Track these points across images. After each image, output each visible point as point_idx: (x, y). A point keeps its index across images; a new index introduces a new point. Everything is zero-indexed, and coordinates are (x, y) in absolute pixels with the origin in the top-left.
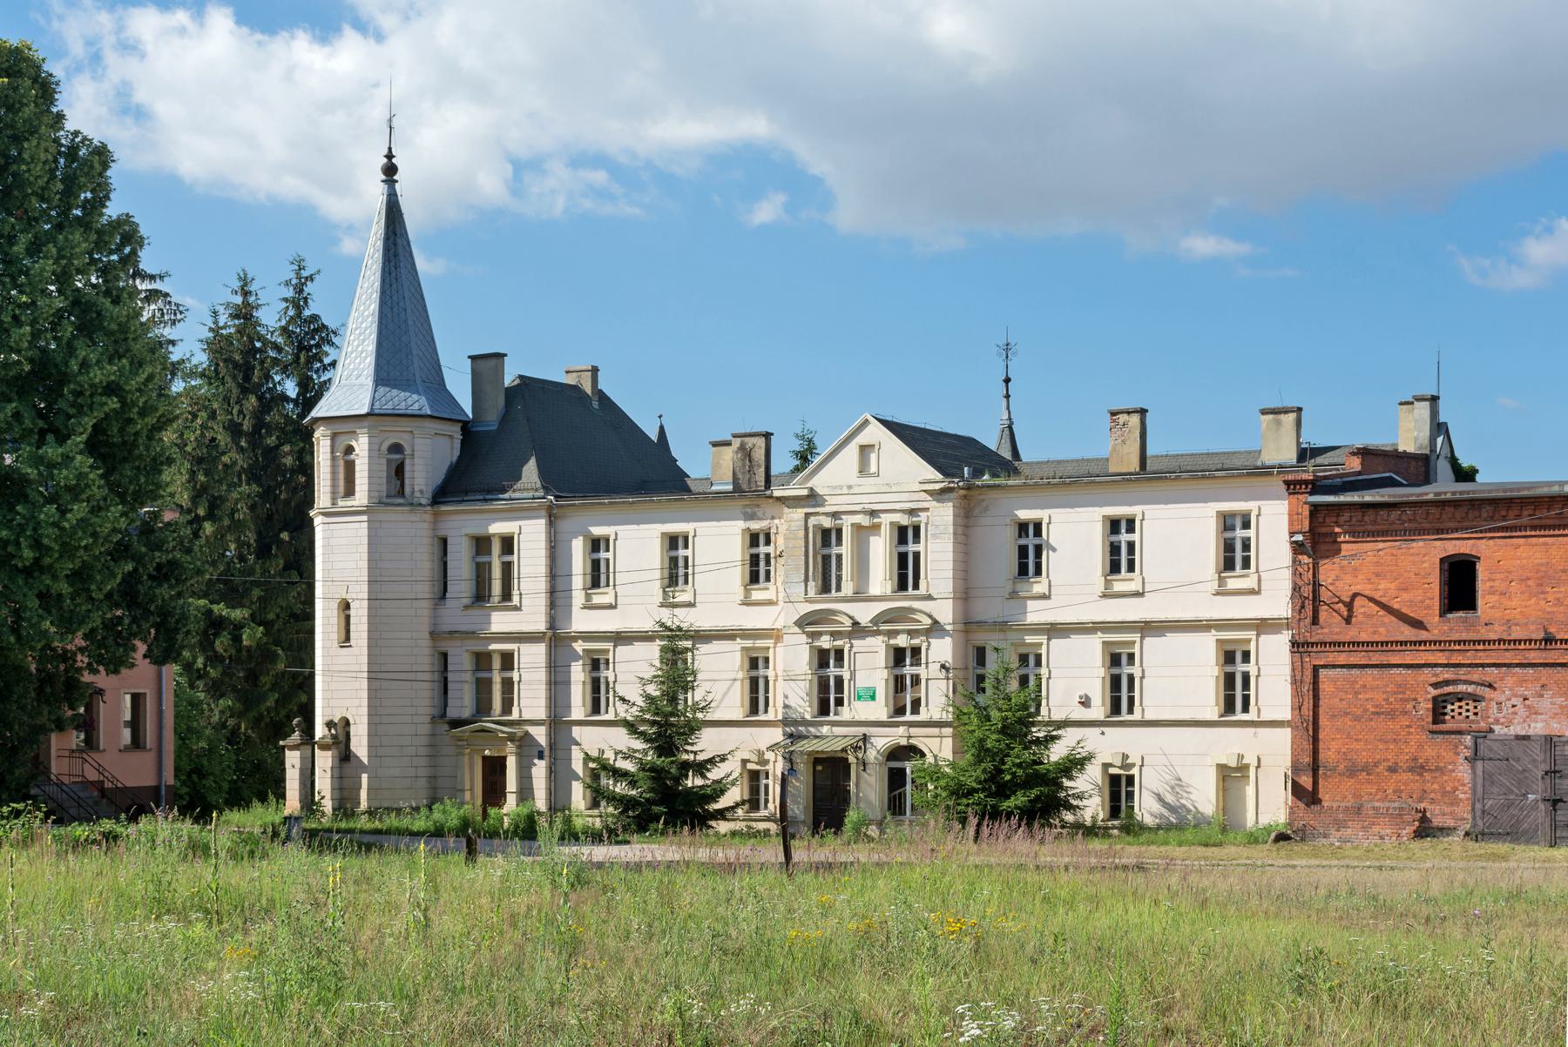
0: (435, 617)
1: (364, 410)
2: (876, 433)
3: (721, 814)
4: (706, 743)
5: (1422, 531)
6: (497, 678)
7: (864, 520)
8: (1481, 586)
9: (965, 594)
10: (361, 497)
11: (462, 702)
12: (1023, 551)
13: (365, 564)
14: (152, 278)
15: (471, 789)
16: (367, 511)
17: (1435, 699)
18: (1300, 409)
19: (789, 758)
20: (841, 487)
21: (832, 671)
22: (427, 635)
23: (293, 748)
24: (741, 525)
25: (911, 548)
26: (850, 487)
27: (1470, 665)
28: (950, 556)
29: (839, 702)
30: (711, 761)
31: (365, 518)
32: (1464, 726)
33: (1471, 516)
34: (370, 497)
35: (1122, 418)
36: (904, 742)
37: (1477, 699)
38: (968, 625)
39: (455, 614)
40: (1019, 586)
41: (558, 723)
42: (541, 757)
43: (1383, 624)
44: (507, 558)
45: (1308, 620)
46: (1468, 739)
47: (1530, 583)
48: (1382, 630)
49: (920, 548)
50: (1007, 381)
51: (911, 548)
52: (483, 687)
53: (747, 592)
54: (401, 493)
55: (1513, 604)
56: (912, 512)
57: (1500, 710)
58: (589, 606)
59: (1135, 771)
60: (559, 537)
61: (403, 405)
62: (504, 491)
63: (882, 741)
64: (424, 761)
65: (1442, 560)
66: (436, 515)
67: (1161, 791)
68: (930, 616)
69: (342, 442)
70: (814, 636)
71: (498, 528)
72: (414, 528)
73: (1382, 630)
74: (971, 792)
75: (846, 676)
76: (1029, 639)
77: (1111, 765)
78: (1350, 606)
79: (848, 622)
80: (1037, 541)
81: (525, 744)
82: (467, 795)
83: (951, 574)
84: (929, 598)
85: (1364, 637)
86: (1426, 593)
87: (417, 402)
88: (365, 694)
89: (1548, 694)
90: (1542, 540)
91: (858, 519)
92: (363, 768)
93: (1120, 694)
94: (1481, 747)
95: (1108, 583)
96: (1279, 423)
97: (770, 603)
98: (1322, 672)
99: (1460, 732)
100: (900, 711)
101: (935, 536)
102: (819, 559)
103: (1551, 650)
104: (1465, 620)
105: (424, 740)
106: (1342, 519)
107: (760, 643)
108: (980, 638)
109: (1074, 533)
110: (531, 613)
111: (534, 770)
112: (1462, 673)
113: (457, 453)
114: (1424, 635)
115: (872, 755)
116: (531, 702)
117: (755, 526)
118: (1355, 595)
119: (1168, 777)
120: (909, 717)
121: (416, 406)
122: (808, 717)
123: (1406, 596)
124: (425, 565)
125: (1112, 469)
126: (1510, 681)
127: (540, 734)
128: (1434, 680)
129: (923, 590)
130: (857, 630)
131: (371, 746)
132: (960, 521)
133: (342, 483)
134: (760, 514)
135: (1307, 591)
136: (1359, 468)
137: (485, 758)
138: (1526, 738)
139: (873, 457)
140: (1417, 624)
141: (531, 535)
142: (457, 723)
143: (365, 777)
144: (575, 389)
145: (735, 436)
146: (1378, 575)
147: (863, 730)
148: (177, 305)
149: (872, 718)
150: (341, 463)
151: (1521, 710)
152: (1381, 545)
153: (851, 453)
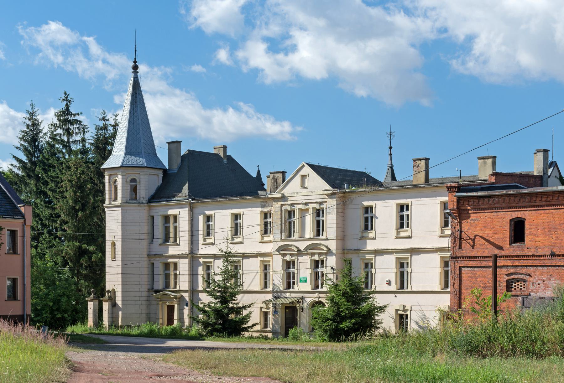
0: (150, 249)
1: (119, 165)
2: (307, 170)
3: (246, 329)
4: (241, 300)
5: (502, 208)
6: (172, 273)
7: (302, 207)
8: (527, 232)
9: (342, 237)
10: (119, 201)
11: (159, 284)
12: (366, 219)
13: (120, 227)
14: (75, 115)
15: (162, 319)
16: (121, 206)
17: (507, 281)
18: (494, 157)
19: (275, 306)
20: (294, 193)
21: (291, 270)
22: (146, 256)
23: (91, 301)
24: (260, 209)
25: (321, 218)
26: (297, 193)
27: (521, 266)
28: (335, 222)
29: (294, 283)
30: (244, 307)
31: (120, 208)
32: (519, 293)
33: (522, 201)
34: (122, 200)
35: (418, 162)
36: (317, 300)
37: (525, 281)
38: (344, 251)
39: (156, 249)
40: (364, 234)
41: (193, 292)
42: (187, 305)
43: (487, 249)
44: (175, 225)
45: (457, 247)
46: (520, 299)
47: (546, 230)
48: (486, 251)
49: (324, 218)
50: (391, 148)
51: (321, 218)
52: (167, 277)
53: (262, 237)
54: (136, 199)
55: (539, 239)
56: (321, 203)
57: (533, 286)
58: (205, 244)
59: (408, 313)
60: (195, 215)
61: (135, 163)
62: (174, 197)
63: (310, 299)
64: (144, 307)
65: (511, 220)
66: (150, 207)
67: (418, 320)
68: (327, 247)
69: (113, 178)
70: (284, 255)
71: (171, 212)
72: (140, 213)
73: (486, 251)
74: (328, 319)
75: (296, 272)
76: (368, 256)
77: (399, 310)
78: (474, 240)
79: (296, 250)
80: (371, 215)
81: (181, 300)
82: (161, 321)
83: (335, 229)
84: (327, 239)
85: (479, 254)
86: (504, 235)
87: (141, 161)
88: (120, 280)
89: (553, 279)
90: (551, 211)
91: (301, 206)
92: (120, 309)
93: (403, 278)
94: (525, 302)
95: (398, 233)
96: (485, 163)
97: (270, 242)
98: (463, 270)
99: (517, 296)
100: (317, 287)
101: (329, 213)
102: (287, 224)
103: (553, 258)
104: (520, 247)
105: (145, 298)
106: (470, 203)
107: (266, 259)
108: (349, 256)
109: (385, 211)
110: (183, 248)
111: (184, 311)
112: (518, 270)
113: (161, 182)
114: (502, 253)
115: (305, 305)
116: (184, 284)
117: (265, 210)
118: (476, 236)
119: (420, 315)
120: (320, 289)
121: (141, 163)
122: (281, 289)
123: (496, 236)
124: (145, 227)
125: (414, 183)
126: (537, 273)
127: (186, 296)
128: (507, 273)
129: (325, 236)
130: (300, 253)
131: (123, 301)
132: (340, 206)
133: (113, 195)
134: (267, 205)
135: (457, 234)
136: (494, 181)
137: (168, 306)
138: (542, 298)
139: (306, 180)
140: (500, 248)
141: (183, 214)
142: (157, 291)
143: (120, 312)
144: (217, 155)
145: (271, 173)
146: (485, 227)
147: (300, 295)
148: (84, 125)
149: (305, 290)
150: (113, 187)
151: (542, 286)
152: (486, 214)
153: (298, 179)
